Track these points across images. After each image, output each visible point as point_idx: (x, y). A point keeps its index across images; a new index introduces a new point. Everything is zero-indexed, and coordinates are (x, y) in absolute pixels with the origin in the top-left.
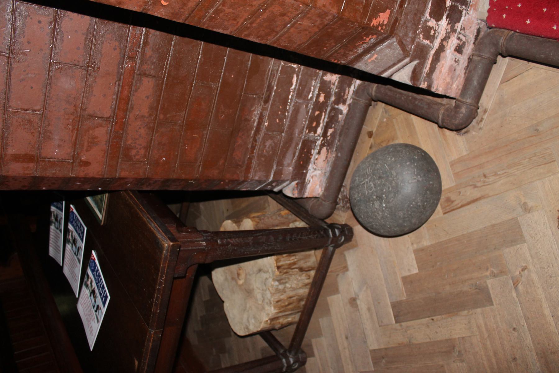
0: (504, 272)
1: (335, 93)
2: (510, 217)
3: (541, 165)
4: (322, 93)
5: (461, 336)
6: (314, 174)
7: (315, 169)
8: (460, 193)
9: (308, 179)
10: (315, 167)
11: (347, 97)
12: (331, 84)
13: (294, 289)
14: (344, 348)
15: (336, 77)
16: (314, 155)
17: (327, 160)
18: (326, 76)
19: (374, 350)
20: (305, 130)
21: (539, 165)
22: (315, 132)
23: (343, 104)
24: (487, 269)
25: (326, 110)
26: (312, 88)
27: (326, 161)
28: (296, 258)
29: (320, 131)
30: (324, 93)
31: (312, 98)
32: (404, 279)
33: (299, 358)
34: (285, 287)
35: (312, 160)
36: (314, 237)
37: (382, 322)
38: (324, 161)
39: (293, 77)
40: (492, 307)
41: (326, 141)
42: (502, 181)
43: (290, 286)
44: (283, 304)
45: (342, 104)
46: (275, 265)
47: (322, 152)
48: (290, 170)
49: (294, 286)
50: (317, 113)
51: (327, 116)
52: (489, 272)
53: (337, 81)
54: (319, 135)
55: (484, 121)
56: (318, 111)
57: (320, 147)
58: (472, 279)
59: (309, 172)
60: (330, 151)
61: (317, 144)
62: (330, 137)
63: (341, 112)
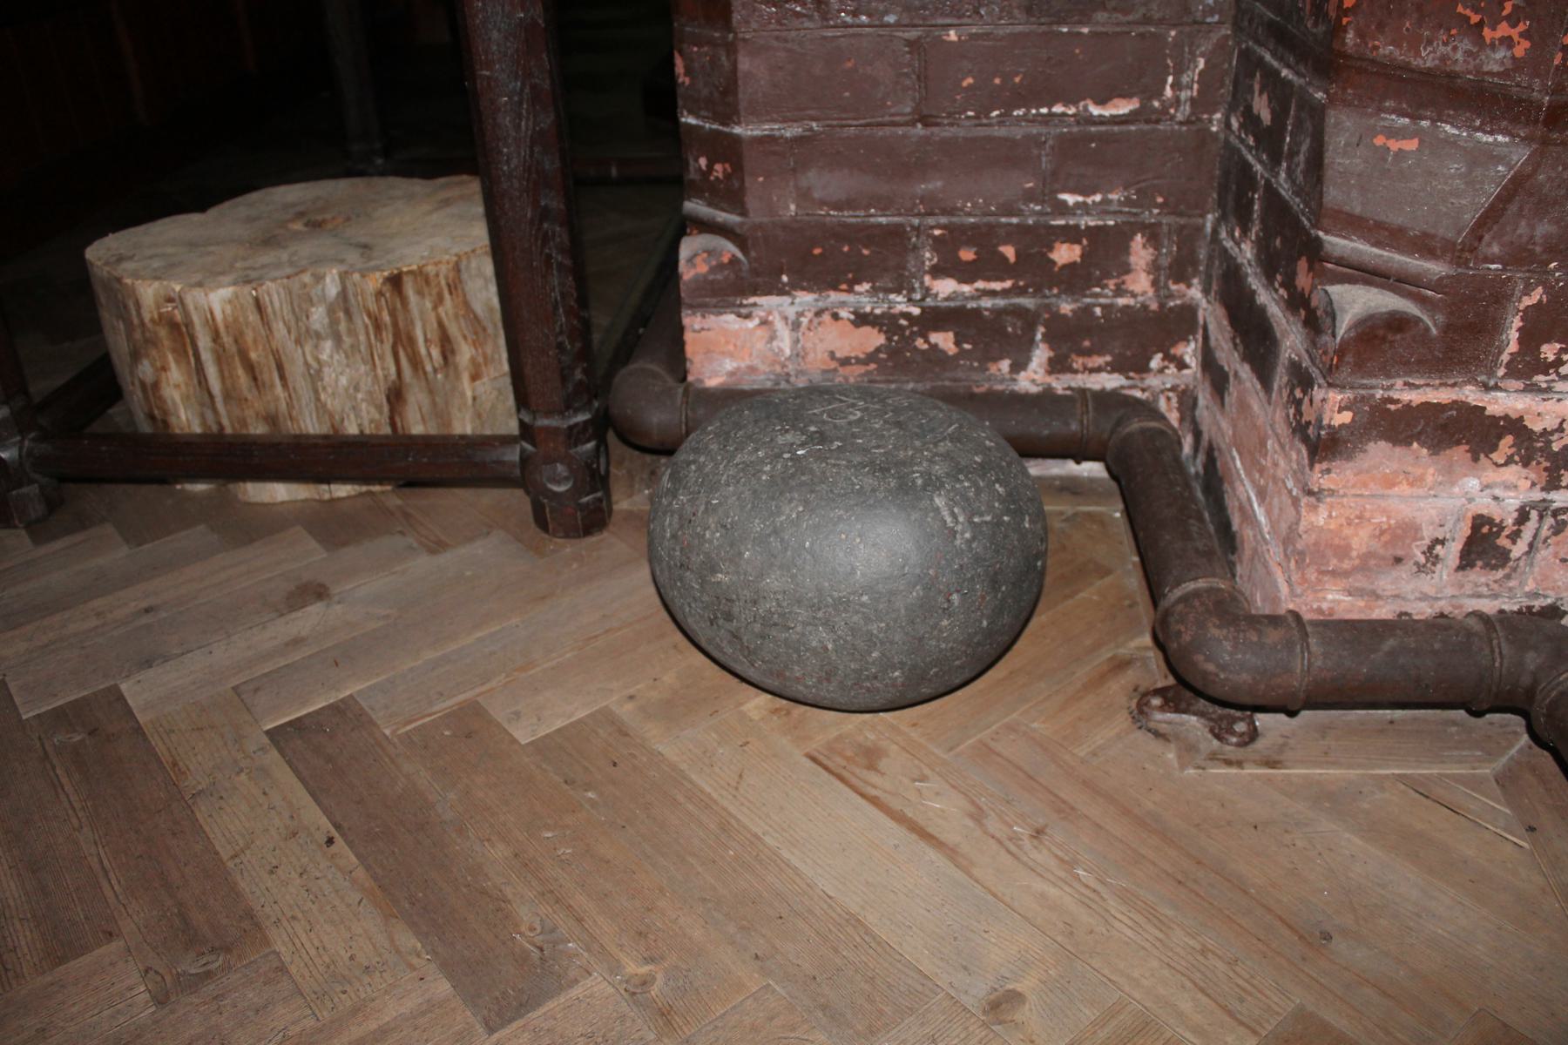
0: (669, 1023)
1: (1088, 309)
2: (927, 966)
3: (1208, 995)
4: (1083, 249)
5: (286, 958)
6: (779, 325)
7: (796, 326)
8: (923, 779)
9: (755, 305)
10: (804, 320)
11: (1076, 372)
12: (1118, 277)
13: (315, 377)
14: (98, 615)
15: (1144, 293)
16: (851, 298)
17: (835, 370)
18: (1144, 246)
19: (121, 698)
20: (943, 220)
21: (1202, 991)
22: (937, 272)
23: (1050, 360)
24: (650, 960)
25: (1021, 292)
26: (1098, 198)
27: (833, 365)
28: (435, 371)
29: (945, 287)
30: (1082, 256)
31: (1063, 210)
32: (473, 711)
33: (20, 485)
34: (318, 336)
35: (834, 297)
36: (561, 332)
37: (256, 690)
38: (832, 354)
39: (1126, 96)
40: (480, 1029)
41: (907, 333)
42: (1053, 892)
43: (324, 357)
44: (249, 337)
45: (1052, 354)
46: (405, 269)
47: (867, 329)
48: (788, 208)
49: (328, 375)
50: (1009, 252)
51: (1000, 302)
52: (645, 969)
53: (1131, 302)
54: (927, 292)
55: (1233, 771)
56: (1018, 255)
57: (883, 315)
58: (580, 920)
59: (786, 300)
60: (873, 366)
61: (892, 296)
62: (926, 346)
63: (1019, 366)
